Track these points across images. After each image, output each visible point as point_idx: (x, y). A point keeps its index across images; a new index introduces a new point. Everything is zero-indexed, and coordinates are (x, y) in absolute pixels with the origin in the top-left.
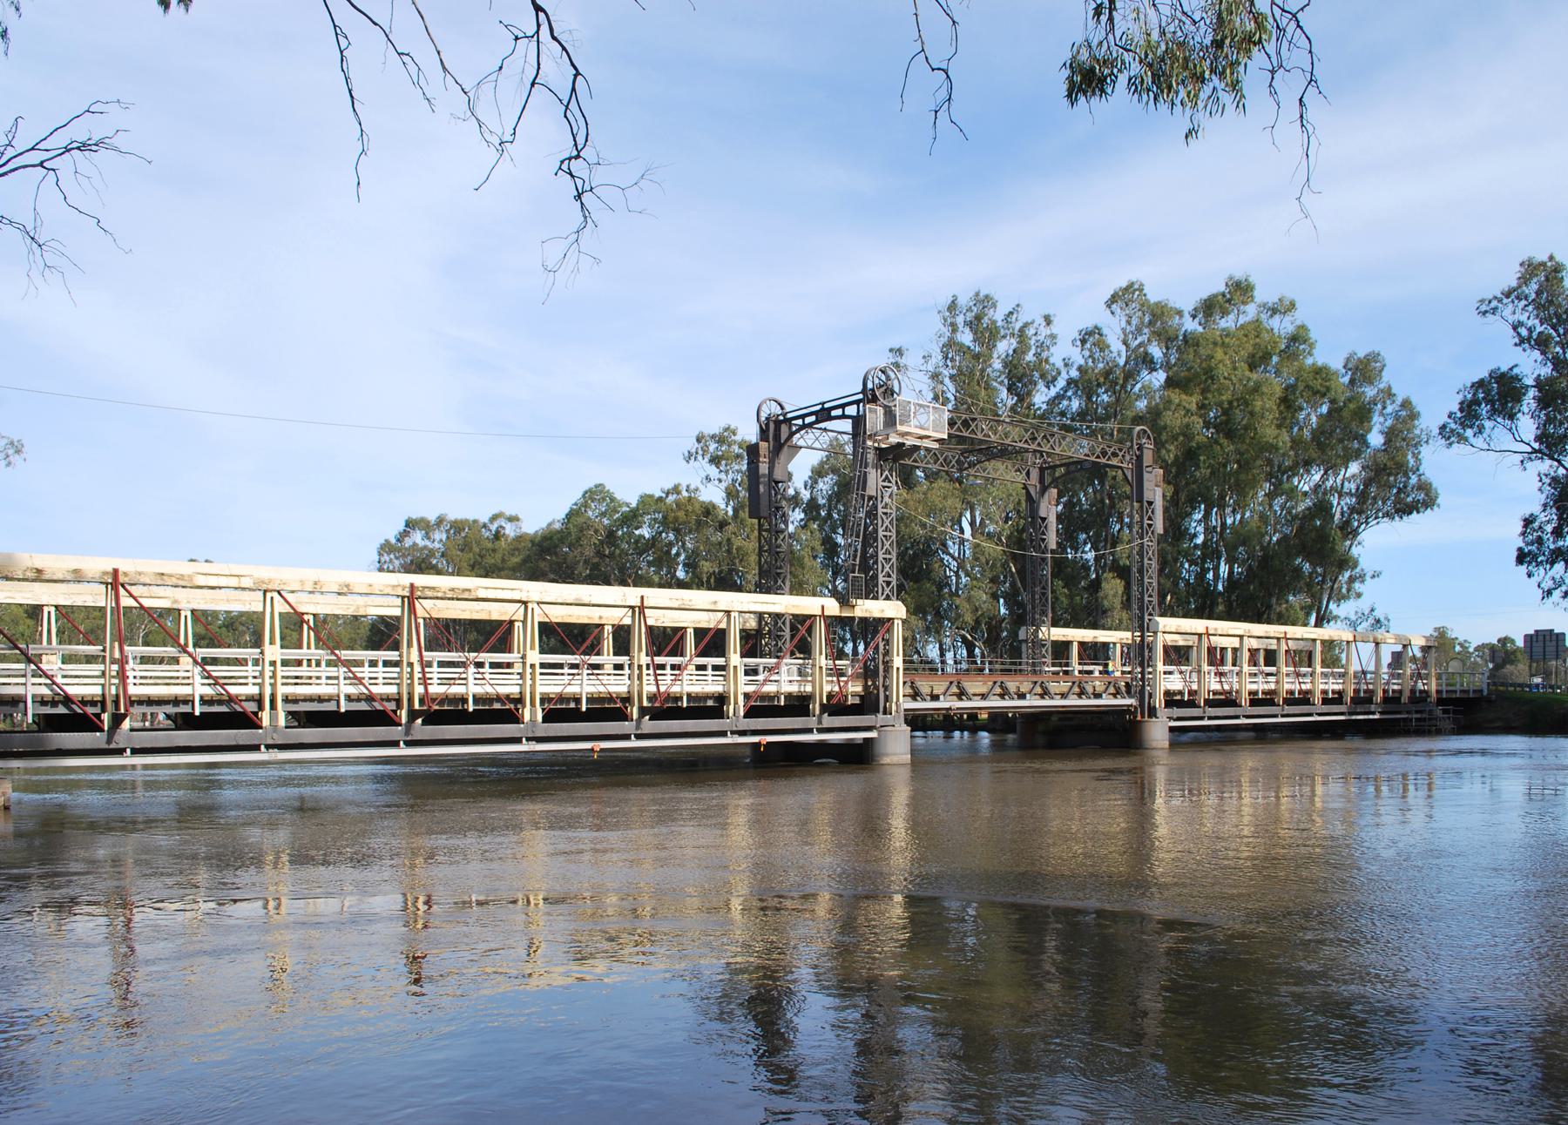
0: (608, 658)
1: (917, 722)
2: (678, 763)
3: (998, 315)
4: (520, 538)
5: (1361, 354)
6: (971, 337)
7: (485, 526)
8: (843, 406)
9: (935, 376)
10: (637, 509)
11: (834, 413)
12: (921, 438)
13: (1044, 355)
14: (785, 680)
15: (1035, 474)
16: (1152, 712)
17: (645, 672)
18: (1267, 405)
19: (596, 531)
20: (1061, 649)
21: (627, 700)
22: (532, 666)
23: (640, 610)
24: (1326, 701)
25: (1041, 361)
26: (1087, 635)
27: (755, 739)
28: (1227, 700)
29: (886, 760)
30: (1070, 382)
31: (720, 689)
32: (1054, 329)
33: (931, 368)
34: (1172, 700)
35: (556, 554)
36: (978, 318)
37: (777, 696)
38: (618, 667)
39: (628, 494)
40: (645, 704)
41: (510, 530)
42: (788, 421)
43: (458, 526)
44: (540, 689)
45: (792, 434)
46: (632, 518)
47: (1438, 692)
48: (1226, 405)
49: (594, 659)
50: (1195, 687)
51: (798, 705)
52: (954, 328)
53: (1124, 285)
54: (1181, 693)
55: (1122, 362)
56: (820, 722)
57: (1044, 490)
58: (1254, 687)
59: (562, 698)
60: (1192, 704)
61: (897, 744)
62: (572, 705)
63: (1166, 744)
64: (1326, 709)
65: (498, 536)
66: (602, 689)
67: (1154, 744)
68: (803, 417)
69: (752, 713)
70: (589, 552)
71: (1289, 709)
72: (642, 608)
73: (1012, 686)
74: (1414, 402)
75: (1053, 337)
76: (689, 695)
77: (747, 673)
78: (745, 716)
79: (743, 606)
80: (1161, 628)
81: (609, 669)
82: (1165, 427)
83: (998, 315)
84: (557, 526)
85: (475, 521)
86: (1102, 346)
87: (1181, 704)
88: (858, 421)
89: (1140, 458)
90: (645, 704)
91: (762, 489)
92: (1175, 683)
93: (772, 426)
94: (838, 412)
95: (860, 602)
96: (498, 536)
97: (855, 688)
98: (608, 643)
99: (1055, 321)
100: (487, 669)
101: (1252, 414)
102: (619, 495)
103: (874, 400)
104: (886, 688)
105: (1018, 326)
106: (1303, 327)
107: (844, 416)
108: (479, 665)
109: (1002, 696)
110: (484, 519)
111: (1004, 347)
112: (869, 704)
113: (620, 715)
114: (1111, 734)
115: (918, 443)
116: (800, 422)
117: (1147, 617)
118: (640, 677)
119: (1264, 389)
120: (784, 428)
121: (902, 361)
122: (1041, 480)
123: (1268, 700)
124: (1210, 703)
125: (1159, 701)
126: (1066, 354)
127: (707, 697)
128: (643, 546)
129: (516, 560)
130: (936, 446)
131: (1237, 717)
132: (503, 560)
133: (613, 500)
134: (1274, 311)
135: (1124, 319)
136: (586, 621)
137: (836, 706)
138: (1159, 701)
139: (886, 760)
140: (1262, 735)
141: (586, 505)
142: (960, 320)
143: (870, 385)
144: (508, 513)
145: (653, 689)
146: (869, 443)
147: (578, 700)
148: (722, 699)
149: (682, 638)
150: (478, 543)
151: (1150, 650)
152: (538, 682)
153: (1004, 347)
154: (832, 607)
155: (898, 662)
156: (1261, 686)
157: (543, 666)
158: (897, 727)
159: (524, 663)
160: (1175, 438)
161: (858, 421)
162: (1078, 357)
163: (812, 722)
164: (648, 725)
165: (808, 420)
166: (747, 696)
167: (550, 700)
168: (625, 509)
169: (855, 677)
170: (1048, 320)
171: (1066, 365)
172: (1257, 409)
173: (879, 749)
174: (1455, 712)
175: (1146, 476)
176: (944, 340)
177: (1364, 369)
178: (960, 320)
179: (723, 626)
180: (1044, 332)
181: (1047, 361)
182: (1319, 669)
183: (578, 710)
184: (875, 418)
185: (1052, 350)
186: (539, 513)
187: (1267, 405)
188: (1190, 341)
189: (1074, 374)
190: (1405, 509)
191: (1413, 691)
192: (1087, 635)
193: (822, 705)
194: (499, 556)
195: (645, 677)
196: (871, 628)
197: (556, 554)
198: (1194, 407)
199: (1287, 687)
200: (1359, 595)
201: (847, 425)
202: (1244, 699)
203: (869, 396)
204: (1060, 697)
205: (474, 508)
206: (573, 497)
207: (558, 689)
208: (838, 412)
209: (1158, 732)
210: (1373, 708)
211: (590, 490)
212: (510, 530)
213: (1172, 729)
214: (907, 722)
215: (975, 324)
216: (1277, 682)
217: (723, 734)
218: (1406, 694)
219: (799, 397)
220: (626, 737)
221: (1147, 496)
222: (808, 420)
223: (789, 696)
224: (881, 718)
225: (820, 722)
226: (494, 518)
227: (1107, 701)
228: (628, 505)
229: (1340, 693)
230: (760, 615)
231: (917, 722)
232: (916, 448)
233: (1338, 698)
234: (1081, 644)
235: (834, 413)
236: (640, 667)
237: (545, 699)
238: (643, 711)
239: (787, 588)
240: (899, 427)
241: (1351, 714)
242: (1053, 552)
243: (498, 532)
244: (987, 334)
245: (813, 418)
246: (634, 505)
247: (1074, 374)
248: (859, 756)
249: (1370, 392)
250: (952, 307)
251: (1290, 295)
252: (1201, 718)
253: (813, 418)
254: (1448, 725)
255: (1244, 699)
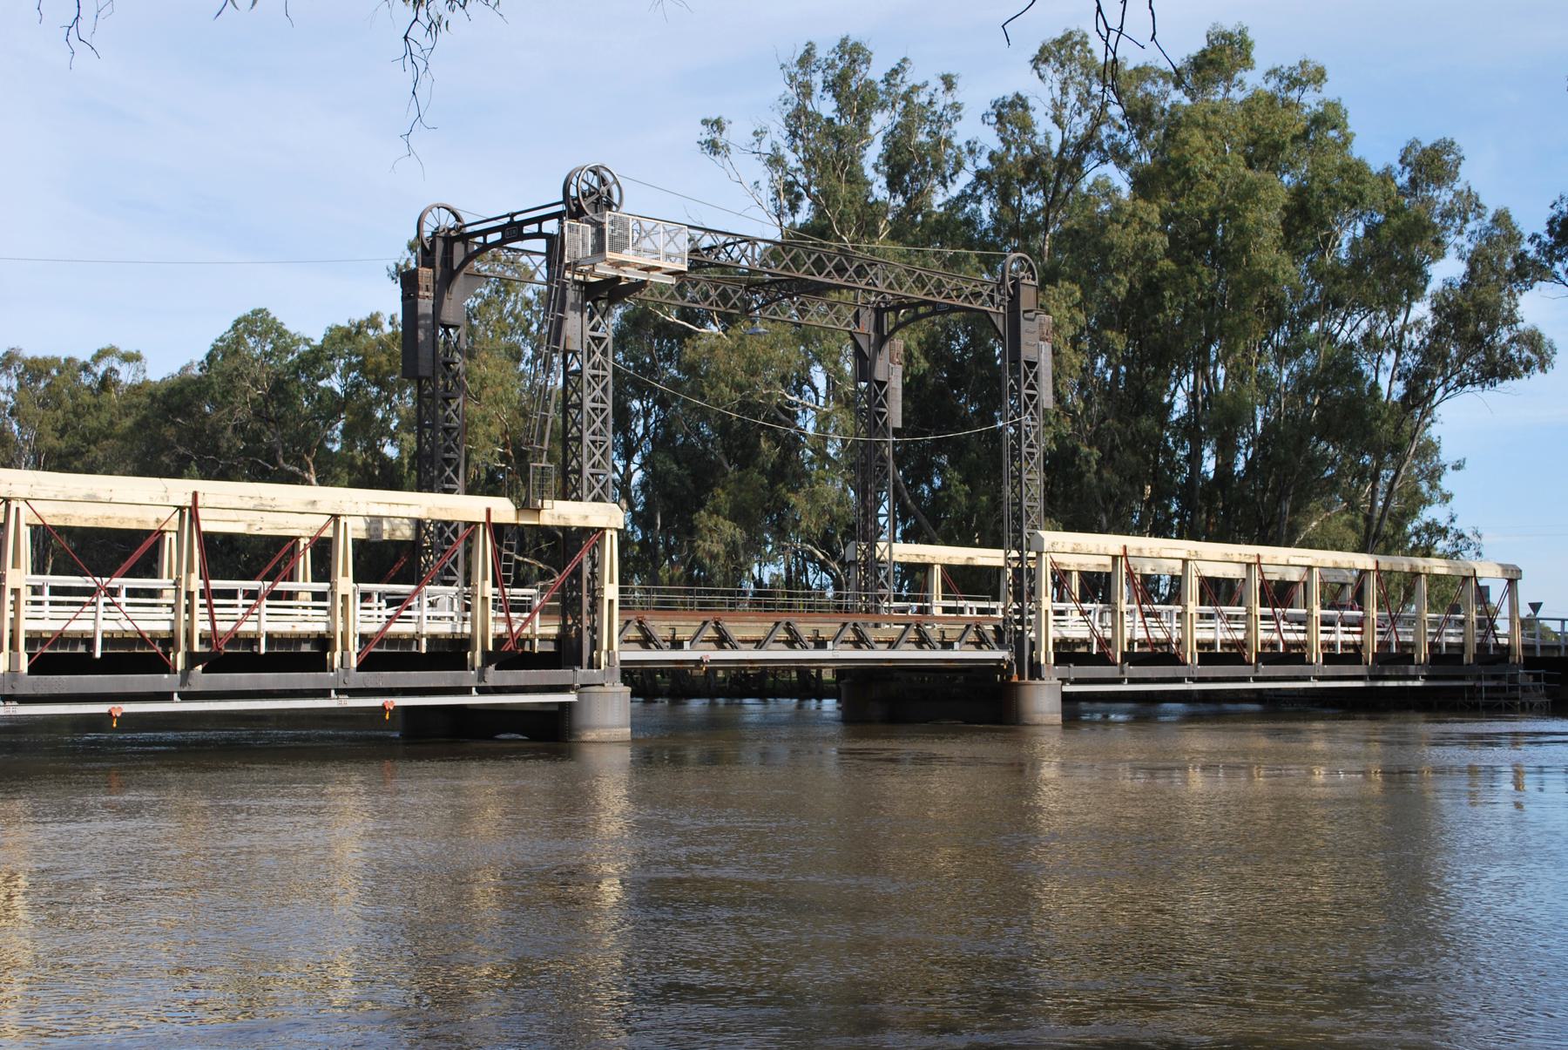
0: (304, 585)
1: (641, 681)
2: (241, 731)
3: (875, 72)
4: (135, 389)
5: (1427, 144)
6: (834, 105)
7: (85, 367)
8: (539, 220)
9: (775, 161)
10: (321, 349)
11: (528, 229)
12: (647, 269)
13: (944, 133)
14: (433, 614)
15: (867, 318)
16: (1036, 671)
17: (198, 601)
18: (1266, 218)
19: (255, 382)
20: (915, 574)
21: (169, 642)
22: (16, 592)
23: (191, 513)
24: (1330, 659)
25: (940, 143)
26: (958, 555)
27: (376, 702)
28: (1161, 655)
29: (591, 735)
30: (980, 176)
31: (321, 628)
32: (959, 95)
33: (766, 148)
34: (1067, 653)
35: (190, 415)
36: (843, 78)
37: (415, 639)
38: (318, 596)
39: (309, 323)
40: (197, 648)
41: (126, 374)
42: (465, 238)
43: (36, 369)
44: (25, 626)
45: (470, 257)
46: (315, 360)
47: (1525, 647)
48: (1206, 216)
49: (282, 586)
50: (1108, 634)
51: (450, 653)
52: (806, 90)
53: (1059, 35)
54: (1084, 642)
55: (1055, 147)
56: (482, 678)
57: (882, 340)
58: (1208, 636)
59: (61, 638)
60: (1103, 659)
61: (610, 714)
62: (81, 649)
63: (1058, 718)
64: (1330, 670)
65: (106, 383)
66: (128, 626)
67: (1038, 718)
68: (484, 233)
69: (369, 663)
70: (243, 413)
71: (1264, 670)
72: (194, 509)
73: (805, 629)
74: (1515, 218)
75: (956, 107)
76: (269, 636)
77: (1323, 624)
78: (359, 669)
79: (359, 509)
80: (1047, 546)
81: (305, 599)
82: (1111, 247)
83: (875, 72)
84: (196, 371)
85: (69, 361)
86: (1026, 127)
87: (1087, 659)
88: (555, 245)
89: (1015, 300)
90: (197, 648)
91: (421, 335)
92: (1075, 629)
93: (440, 245)
94: (534, 228)
95: (547, 503)
96: (106, 383)
97: (544, 629)
98: (304, 563)
99: (960, 84)
100: (122, 598)
101: (1241, 230)
102: (293, 326)
103: (577, 214)
104: (594, 630)
105: (903, 89)
106: (1334, 106)
107: (539, 235)
108: (113, 592)
109: (790, 644)
110: (84, 356)
111: (881, 122)
112: (566, 652)
113: (159, 665)
114: (977, 700)
115: (642, 276)
116: (480, 239)
117: (1025, 531)
118: (189, 609)
119: (1262, 194)
120: (459, 249)
121: (721, 140)
122: (878, 326)
123: (1233, 654)
124: (1131, 658)
125: (1046, 655)
126: (975, 132)
127: (299, 639)
128: (331, 406)
129: (128, 422)
130: (672, 281)
131: (1180, 680)
132: (111, 423)
133: (282, 333)
134: (1294, 82)
135: (1057, 86)
136: (134, 526)
137: (510, 654)
138: (1046, 655)
139: (591, 735)
140: (1209, 708)
141: (238, 340)
142: (817, 79)
143: (573, 193)
144: (123, 349)
145: (207, 626)
146: (568, 275)
147: (90, 642)
148: (323, 642)
149: (293, 553)
150: (73, 396)
151: (1032, 578)
152: (23, 615)
153: (881, 122)
154: (503, 510)
155: (611, 591)
156: (1218, 633)
157: (1201, 616)
158: (608, 687)
159: (177, 590)
160: (1124, 265)
161: (555, 245)
162: (990, 140)
163: (469, 678)
164: (200, 679)
165: (492, 238)
166: (364, 638)
167: (44, 641)
168: (303, 348)
169: (546, 612)
170: (949, 82)
171: (971, 151)
172: (1249, 223)
173: (581, 719)
174: (1547, 678)
175: (1024, 325)
176: (790, 108)
177: (1432, 164)
178: (817, 79)
179: (328, 533)
180: (942, 100)
181: (948, 143)
182: (1318, 611)
183: (89, 655)
184: (579, 239)
185: (956, 126)
186: (170, 349)
187: (1266, 218)
188: (1176, 123)
189: (984, 163)
190: (1497, 370)
191: (1482, 647)
192: (958, 555)
193: (485, 652)
194: (105, 417)
195: (197, 610)
196: (568, 544)
197: (190, 415)
198: (1155, 219)
199: (1263, 636)
200: (1447, 498)
201: (540, 245)
202: (1191, 655)
203: (573, 209)
204: (892, 645)
205: (62, 335)
206: (219, 327)
207: (57, 626)
208: (534, 228)
209: (1043, 700)
210: (1412, 670)
211: (245, 319)
212: (126, 374)
213: (1067, 698)
214: (625, 681)
215: (838, 86)
216: (1248, 629)
217: (324, 694)
218: (1471, 650)
219: (484, 204)
220: (166, 697)
221: (1027, 353)
222: (492, 238)
223: (433, 639)
224: (582, 674)
225: (482, 678)
226: (100, 355)
227: (959, 653)
228: (307, 341)
229: (1357, 647)
230: (419, 524)
231: (641, 681)
232: (642, 284)
233: (1353, 655)
234: (948, 569)
235: (528, 229)
236: (189, 595)
237: (33, 640)
238: (192, 659)
239: (460, 482)
240: (609, 255)
241: (1373, 678)
242: (896, 432)
243: (105, 378)
244: (858, 102)
245: (497, 236)
246: (317, 342)
247: (984, 163)
248: (551, 733)
249: (1444, 196)
250: (806, 59)
251: (1317, 58)
252: (1119, 681)
253: (497, 236)
254: (1539, 698)
255: (1191, 655)
